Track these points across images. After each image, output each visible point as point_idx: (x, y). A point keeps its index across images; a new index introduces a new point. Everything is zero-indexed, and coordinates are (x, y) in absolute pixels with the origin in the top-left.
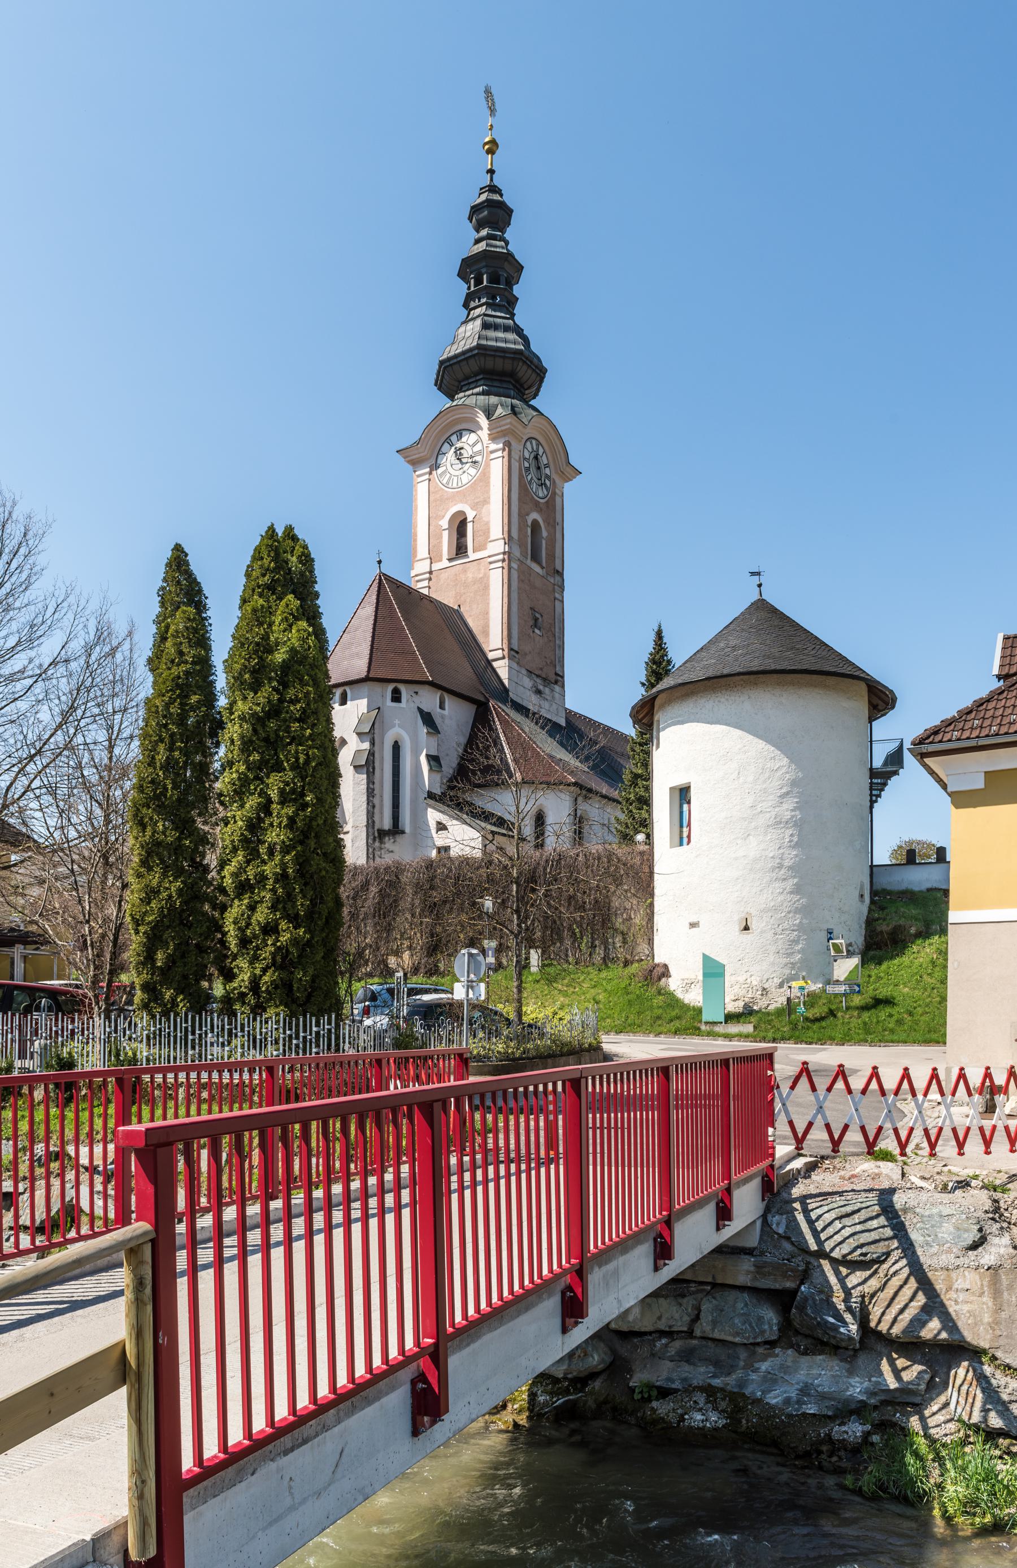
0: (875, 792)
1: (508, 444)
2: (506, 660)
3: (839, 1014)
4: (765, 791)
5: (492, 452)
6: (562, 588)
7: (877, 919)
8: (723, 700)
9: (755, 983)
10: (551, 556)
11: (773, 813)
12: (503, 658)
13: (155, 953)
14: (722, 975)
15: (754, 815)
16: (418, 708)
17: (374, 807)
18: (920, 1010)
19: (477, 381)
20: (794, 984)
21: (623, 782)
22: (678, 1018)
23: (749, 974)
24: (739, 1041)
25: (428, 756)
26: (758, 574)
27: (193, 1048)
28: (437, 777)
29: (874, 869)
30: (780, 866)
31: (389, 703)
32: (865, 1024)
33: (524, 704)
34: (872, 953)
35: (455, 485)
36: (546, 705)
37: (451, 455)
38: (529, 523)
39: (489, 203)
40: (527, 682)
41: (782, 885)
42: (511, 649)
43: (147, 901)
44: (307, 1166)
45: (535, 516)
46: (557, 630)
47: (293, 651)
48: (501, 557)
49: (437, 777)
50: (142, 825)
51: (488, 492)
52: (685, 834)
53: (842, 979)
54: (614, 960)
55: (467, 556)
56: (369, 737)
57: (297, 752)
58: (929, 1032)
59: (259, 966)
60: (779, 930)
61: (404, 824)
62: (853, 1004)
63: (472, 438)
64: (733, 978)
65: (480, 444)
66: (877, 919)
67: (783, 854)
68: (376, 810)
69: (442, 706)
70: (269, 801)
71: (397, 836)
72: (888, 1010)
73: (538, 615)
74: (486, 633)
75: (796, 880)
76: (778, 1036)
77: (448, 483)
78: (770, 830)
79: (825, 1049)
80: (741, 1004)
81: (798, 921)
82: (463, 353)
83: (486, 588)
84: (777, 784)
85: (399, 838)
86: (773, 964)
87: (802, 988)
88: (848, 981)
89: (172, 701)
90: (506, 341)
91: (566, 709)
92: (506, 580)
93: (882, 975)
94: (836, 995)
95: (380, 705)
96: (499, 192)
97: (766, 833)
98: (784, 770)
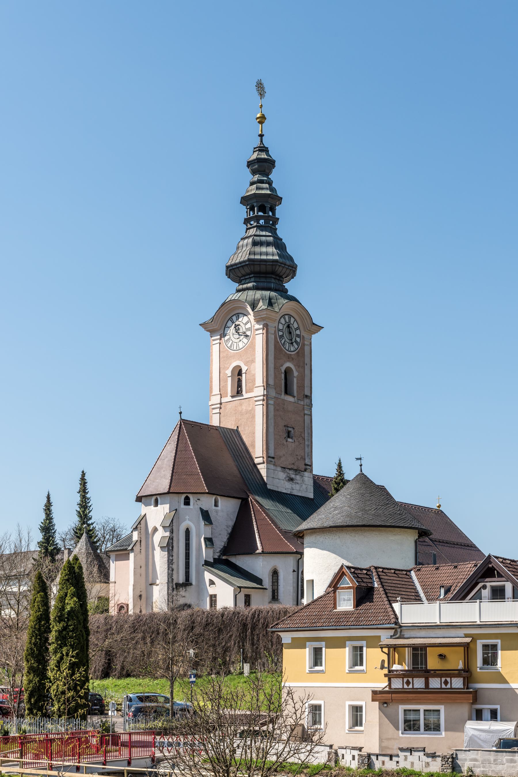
1: (266, 326)
2: (265, 465)
5: (257, 330)
6: (310, 405)
10: (301, 387)
12: (263, 463)
13: (31, 699)
16: (200, 508)
17: (173, 570)
19: (250, 278)
25: (205, 539)
26: (360, 459)
27: (42, 727)
28: (211, 551)
31: (182, 506)
33: (279, 490)
35: (235, 348)
36: (297, 487)
37: (232, 329)
38: (283, 371)
39: (259, 160)
40: (282, 475)
42: (268, 457)
43: (29, 684)
44: (55, 756)
45: (288, 364)
46: (306, 435)
47: (72, 608)
48: (262, 398)
49: (211, 551)
50: (28, 661)
51: (254, 355)
55: (242, 395)
56: (169, 529)
57: (71, 641)
59: (60, 703)
61: (192, 580)
63: (245, 319)
65: (249, 323)
68: (175, 572)
69: (216, 505)
70: (63, 655)
71: (187, 587)
73: (290, 429)
74: (253, 446)
77: (231, 346)
82: (240, 263)
83: (253, 417)
85: (188, 588)
89: (36, 624)
90: (267, 254)
92: (265, 413)
95: (177, 508)
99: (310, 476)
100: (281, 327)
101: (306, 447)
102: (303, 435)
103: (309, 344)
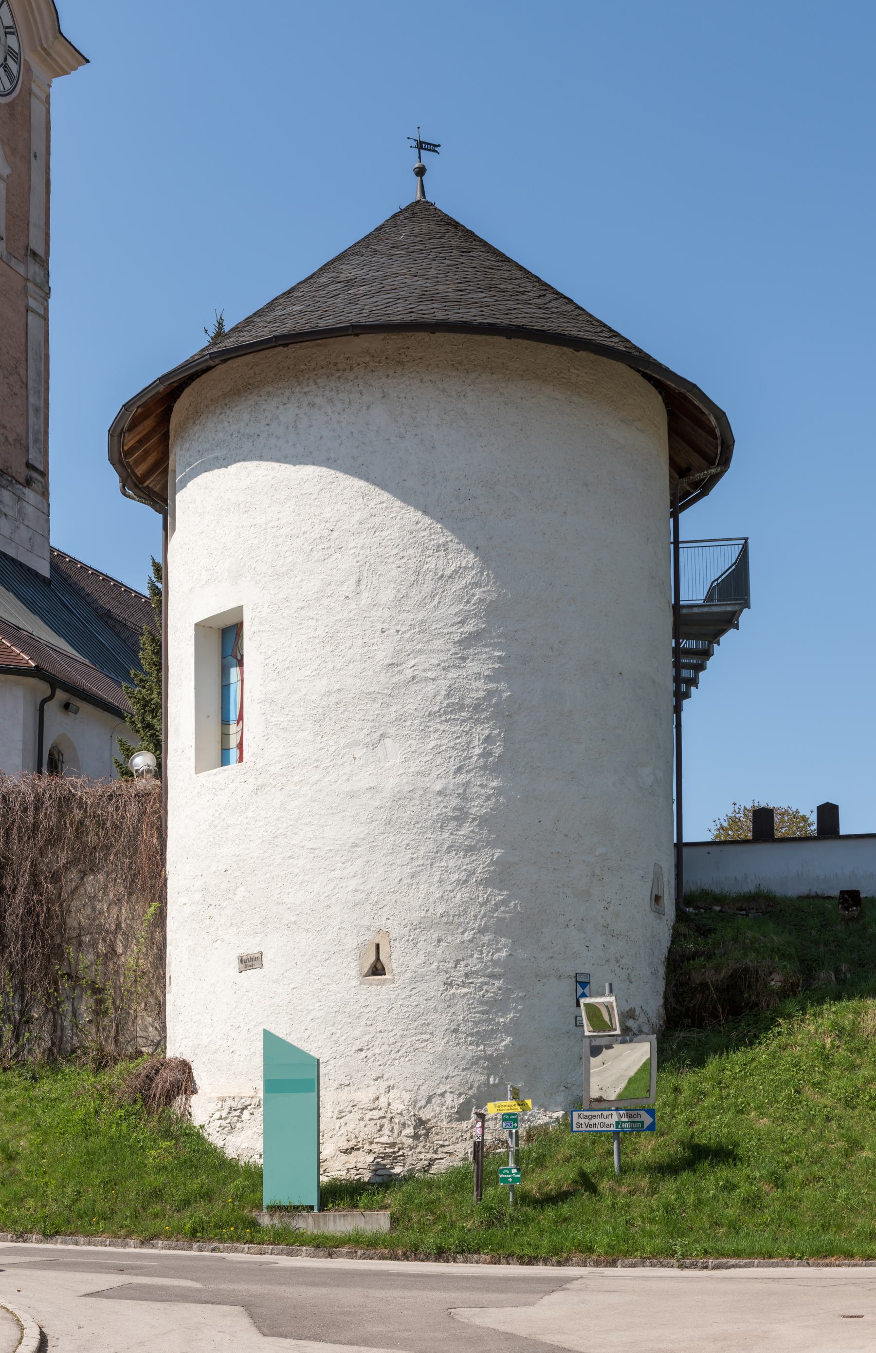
0: (685, 673)
3: (604, 1185)
4: (423, 627)
7: (694, 956)
8: (319, 401)
9: (397, 1106)
11: (443, 684)
14: (313, 1085)
15: (396, 686)
18: (799, 1173)
20: (491, 1109)
21: (139, 666)
22: (207, 1195)
23: (383, 1084)
24: (351, 1255)
26: (433, 148)
29: (685, 851)
30: (461, 816)
32: (668, 1209)
34: (681, 1035)
41: (466, 862)
46: (32, 374)
52: (233, 741)
53: (612, 1095)
54: (71, 1055)
58: (825, 1227)
60: (458, 975)
62: (637, 1159)
64: (345, 1095)
66: (694, 956)
67: (467, 785)
72: (724, 1173)
75: (498, 853)
76: (452, 1242)
78: (435, 724)
79: (561, 1284)
80: (363, 1160)
81: (504, 954)
84: (451, 610)
86: (442, 1059)
87: (510, 1119)
88: (622, 1103)
91: (52, 550)
93: (706, 1086)
94: (597, 1137)
97: (425, 733)
98: (469, 577)
99: (40, 507)
101: (31, 412)
102: (22, 372)
103: (43, 97)
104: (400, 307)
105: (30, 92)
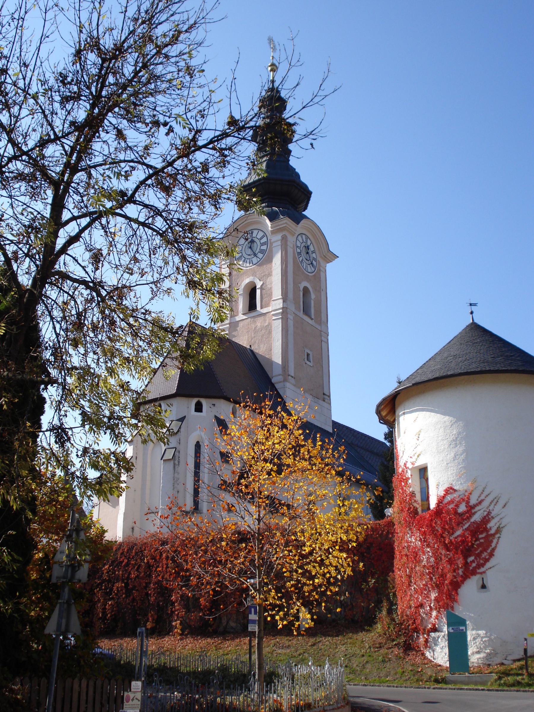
10: (319, 312)
26: (475, 305)
38: (302, 289)
45: (305, 284)
96: (127, 702)
100: (299, 244)
104: (474, 365)
105: (320, 270)
